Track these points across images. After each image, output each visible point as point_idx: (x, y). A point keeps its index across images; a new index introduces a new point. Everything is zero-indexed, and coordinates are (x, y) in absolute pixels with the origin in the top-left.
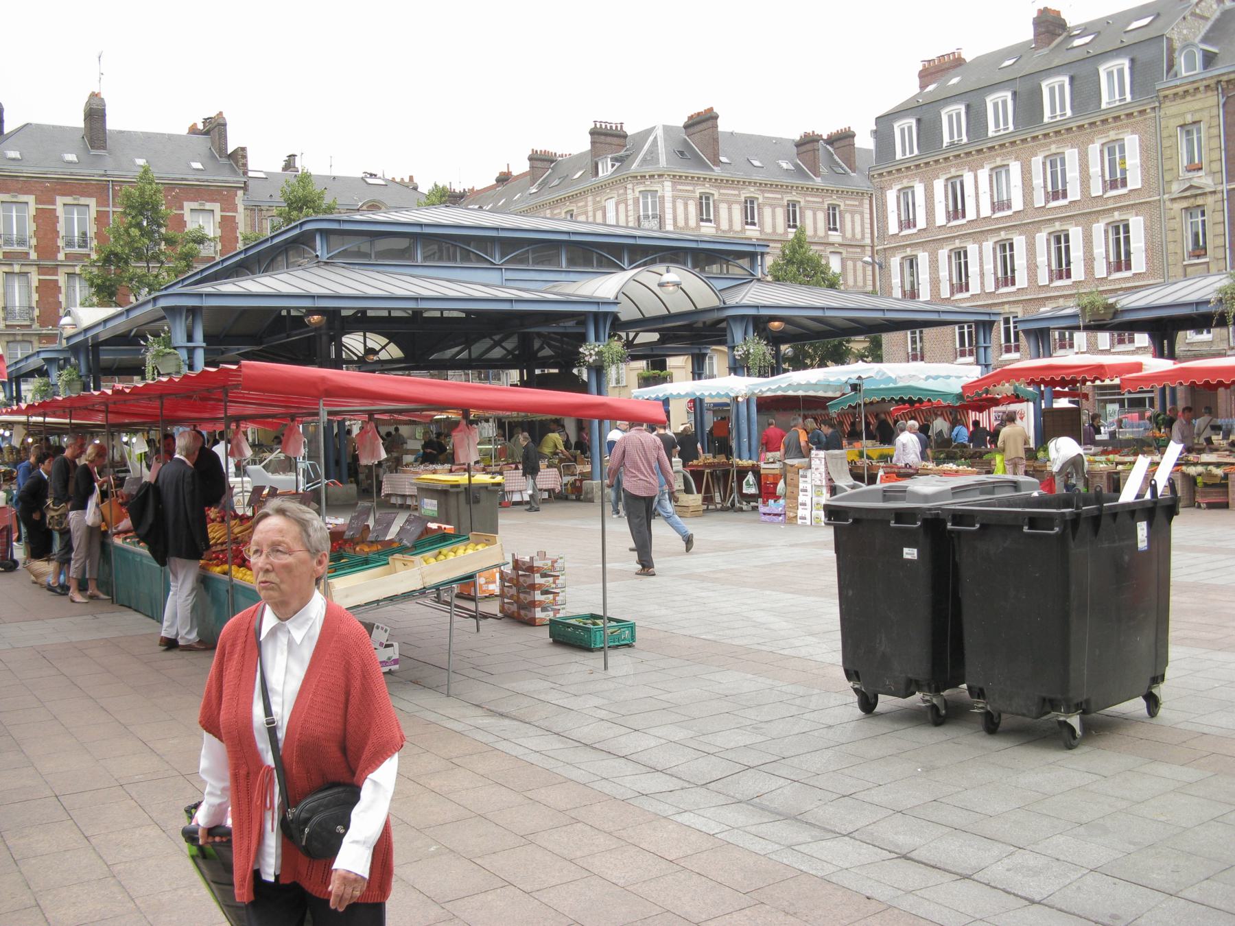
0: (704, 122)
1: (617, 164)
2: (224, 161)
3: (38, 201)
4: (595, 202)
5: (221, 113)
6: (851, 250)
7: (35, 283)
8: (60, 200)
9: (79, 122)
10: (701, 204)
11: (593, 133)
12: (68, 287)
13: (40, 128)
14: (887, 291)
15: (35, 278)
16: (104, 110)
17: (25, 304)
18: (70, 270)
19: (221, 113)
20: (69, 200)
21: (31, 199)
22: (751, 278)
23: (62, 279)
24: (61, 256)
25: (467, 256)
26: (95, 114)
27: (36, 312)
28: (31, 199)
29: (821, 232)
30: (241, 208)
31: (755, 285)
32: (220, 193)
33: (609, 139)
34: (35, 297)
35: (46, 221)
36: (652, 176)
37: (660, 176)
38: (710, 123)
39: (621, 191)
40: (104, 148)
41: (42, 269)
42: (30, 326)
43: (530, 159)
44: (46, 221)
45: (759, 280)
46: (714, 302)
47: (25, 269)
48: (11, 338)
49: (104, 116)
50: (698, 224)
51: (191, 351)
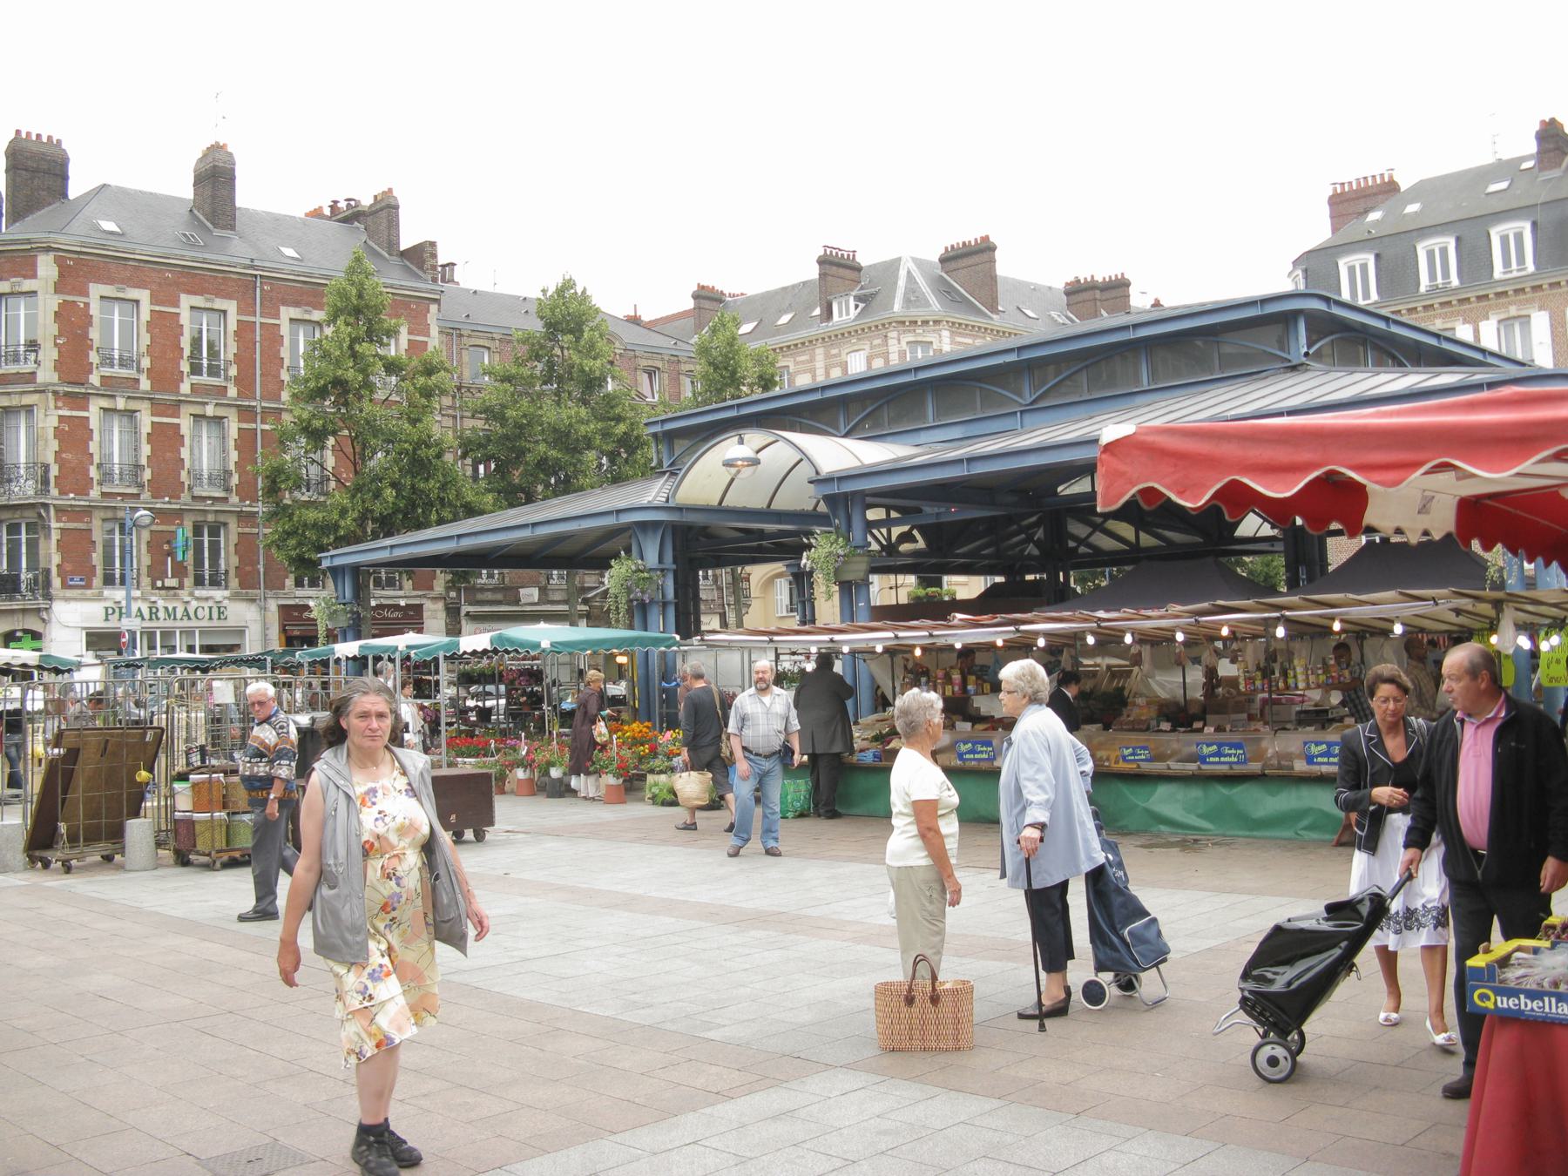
0: (983, 251)
1: (861, 305)
2: (395, 260)
3: (154, 300)
4: (827, 356)
5: (390, 190)
7: (146, 428)
8: (186, 301)
9: (184, 189)
11: (823, 262)
12: (192, 438)
13: (123, 192)
15: (146, 421)
16: (233, 170)
17: (128, 460)
18: (197, 410)
19: (390, 190)
20: (198, 301)
21: (143, 295)
23: (185, 424)
26: (216, 177)
27: (147, 475)
28: (143, 295)
30: (434, 331)
32: (407, 306)
33: (842, 271)
34: (146, 450)
35: (164, 326)
36: (925, 323)
37: (936, 322)
38: (985, 257)
39: (876, 342)
40: (233, 228)
41: (158, 408)
42: (225, 500)
43: (696, 297)
47: (133, 405)
48: (109, 514)
49: (233, 179)
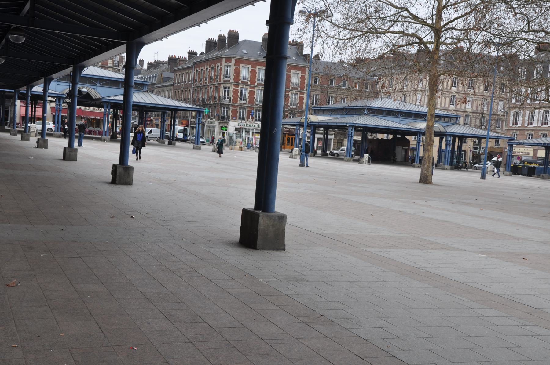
8: (258, 67)
14: (285, 117)
15: (249, 90)
20: (260, 67)
21: (250, 66)
22: (456, 123)
23: (255, 90)
24: (291, 88)
25: (393, 115)
28: (250, 66)
29: (447, 106)
30: (307, 73)
31: (456, 126)
41: (251, 87)
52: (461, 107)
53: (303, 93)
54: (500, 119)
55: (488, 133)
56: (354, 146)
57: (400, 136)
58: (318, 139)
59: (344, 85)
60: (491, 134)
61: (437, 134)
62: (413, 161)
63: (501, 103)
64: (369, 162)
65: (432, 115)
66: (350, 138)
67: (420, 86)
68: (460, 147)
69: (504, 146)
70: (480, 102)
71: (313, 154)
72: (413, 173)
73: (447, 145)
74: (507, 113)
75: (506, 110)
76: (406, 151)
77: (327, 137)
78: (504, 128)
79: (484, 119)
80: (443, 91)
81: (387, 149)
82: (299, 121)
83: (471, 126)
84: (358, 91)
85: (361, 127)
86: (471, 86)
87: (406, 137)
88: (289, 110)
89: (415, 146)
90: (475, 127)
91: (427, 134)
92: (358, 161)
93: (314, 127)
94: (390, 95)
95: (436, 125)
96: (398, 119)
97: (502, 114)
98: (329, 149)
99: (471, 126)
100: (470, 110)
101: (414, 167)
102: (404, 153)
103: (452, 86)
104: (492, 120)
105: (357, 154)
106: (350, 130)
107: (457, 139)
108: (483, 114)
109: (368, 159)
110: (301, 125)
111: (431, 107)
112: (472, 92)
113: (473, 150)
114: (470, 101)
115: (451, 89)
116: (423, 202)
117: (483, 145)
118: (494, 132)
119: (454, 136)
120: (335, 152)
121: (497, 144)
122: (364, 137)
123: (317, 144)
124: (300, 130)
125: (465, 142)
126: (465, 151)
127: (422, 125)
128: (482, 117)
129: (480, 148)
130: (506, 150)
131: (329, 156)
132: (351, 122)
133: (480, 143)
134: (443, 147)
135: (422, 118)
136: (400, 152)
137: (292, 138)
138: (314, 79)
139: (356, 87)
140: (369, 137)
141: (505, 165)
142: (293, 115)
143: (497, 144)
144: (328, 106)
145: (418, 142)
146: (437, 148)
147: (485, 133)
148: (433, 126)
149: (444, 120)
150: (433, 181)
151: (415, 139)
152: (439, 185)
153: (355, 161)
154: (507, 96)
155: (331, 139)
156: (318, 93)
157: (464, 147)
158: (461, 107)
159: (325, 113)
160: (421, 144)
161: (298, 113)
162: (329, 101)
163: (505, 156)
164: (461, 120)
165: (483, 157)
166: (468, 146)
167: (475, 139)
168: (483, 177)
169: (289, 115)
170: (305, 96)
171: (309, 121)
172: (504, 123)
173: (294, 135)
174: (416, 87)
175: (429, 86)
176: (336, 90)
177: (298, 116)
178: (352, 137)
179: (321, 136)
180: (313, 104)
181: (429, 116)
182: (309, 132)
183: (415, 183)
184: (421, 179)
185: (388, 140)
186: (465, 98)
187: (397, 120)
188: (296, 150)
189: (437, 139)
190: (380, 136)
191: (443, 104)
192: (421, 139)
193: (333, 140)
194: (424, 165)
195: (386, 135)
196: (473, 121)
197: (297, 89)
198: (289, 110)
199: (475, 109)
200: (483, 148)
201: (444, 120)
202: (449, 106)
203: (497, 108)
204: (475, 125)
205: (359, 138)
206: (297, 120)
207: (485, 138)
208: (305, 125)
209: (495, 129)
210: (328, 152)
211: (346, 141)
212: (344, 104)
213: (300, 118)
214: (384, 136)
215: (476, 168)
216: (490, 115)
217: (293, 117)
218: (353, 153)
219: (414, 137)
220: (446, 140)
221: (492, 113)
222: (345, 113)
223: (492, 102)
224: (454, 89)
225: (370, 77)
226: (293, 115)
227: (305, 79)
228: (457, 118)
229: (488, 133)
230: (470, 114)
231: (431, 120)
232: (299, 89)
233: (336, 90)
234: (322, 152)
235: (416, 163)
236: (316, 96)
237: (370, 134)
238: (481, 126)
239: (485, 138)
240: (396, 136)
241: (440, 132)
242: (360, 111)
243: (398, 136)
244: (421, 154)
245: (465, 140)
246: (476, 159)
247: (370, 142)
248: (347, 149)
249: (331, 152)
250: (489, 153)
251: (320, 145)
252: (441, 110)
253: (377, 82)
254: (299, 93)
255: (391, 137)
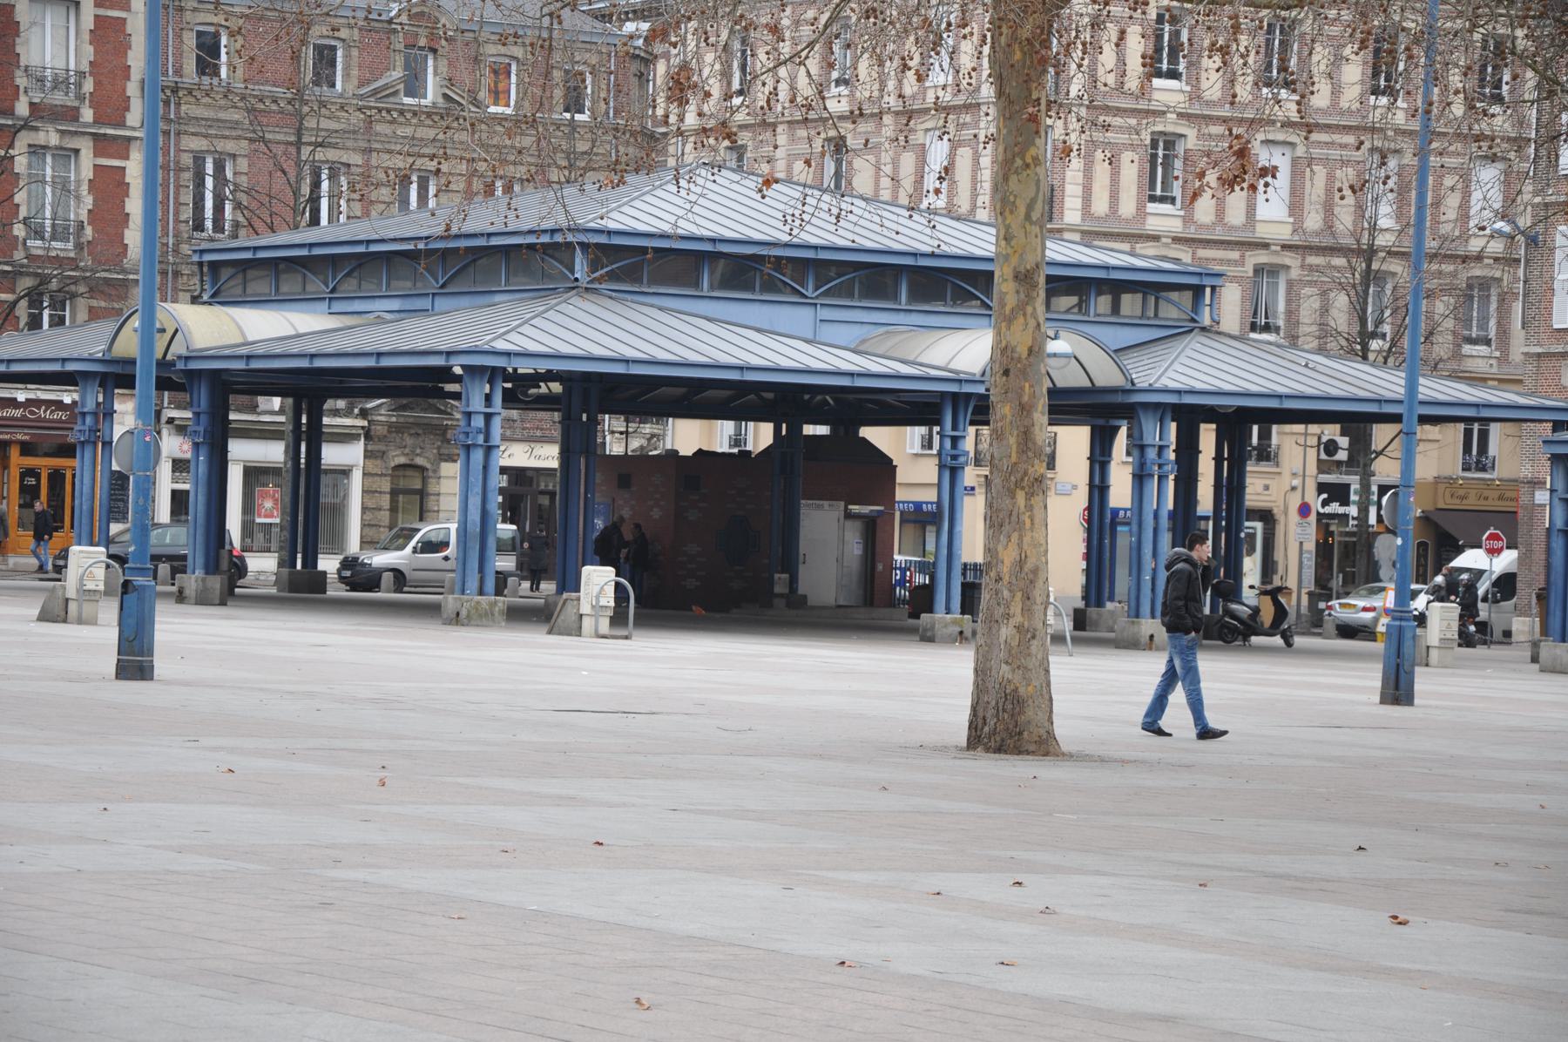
6: (1313, 260)
10: (1154, 157)
24: (22, 108)
25: (770, 286)
29: (1128, 207)
31: (1196, 343)
35: (1022, 191)
44: (1022, 191)
45: (1203, 329)
46: (1116, 380)
50: (1141, 209)
51: (488, 417)
52: (1220, 211)
53: (121, 147)
54: (1485, 284)
55: (1412, 386)
56: (512, 511)
57: (827, 434)
58: (253, 474)
59: (414, 84)
60: (1433, 388)
61: (1069, 405)
62: (923, 600)
63: (1488, 175)
64: (619, 618)
65: (1024, 278)
66: (478, 456)
67: (937, 77)
68: (1231, 488)
69: (1526, 472)
70: (1346, 176)
71: (216, 583)
72: (929, 681)
73: (1140, 478)
74: (1532, 241)
75: (1525, 221)
76: (874, 534)
77: (315, 455)
78: (1519, 345)
79: (1377, 292)
80: (1098, 110)
81: (729, 524)
82: (98, 350)
83: (1293, 340)
84: (519, 123)
85: (550, 376)
86: (1281, 74)
87: (867, 433)
88: (18, 273)
89: (930, 496)
90: (1321, 350)
91: (1003, 411)
92: (541, 616)
93: (216, 394)
94: (739, 151)
95: (1053, 346)
96: (806, 313)
97: (1497, 247)
98: (337, 543)
99: (1293, 340)
100: (1284, 233)
101: (928, 638)
102: (854, 547)
103: (1153, 68)
104: (1430, 295)
105: (533, 571)
106: (477, 404)
107: (1207, 437)
108: (1370, 253)
109: (609, 600)
110: (117, 376)
111: (1015, 222)
112: (1291, 111)
113: (1316, 503)
114: (1271, 171)
115: (1144, 92)
116: (993, 889)
117: (1386, 470)
118: (1456, 376)
119: (1189, 415)
120: (380, 559)
121: (1476, 455)
122: (578, 443)
123: (248, 507)
124: (109, 414)
125: (1265, 454)
126: (1266, 516)
127: (961, 350)
128: (1369, 277)
129: (1365, 487)
130: (1542, 497)
131: (336, 590)
132: (482, 342)
133: (1362, 455)
134: (1120, 493)
135: (963, 296)
136: (826, 538)
137: (57, 478)
138: (190, 40)
139: (498, 95)
140: (615, 447)
141: (1542, 597)
142: (57, 305)
143: (1476, 455)
144: (312, 235)
145: (951, 469)
146: (1081, 499)
147: (1385, 383)
148: (1036, 351)
149: (1116, 309)
150: (1061, 729)
151: (928, 444)
152: (1102, 760)
153: (519, 615)
154: (1521, 122)
155: (345, 472)
156: (230, 146)
157: (1259, 488)
158: (1220, 211)
159: (289, 285)
160: (970, 475)
161: (93, 291)
162: (314, 200)
163: (1539, 534)
164: (1230, 305)
165: (1387, 548)
166: (1287, 481)
167: (1331, 431)
168: (1398, 690)
169: (22, 310)
170: (134, 168)
171: (178, 349)
172: (1518, 308)
173: (68, 451)
174: (910, 85)
175: (999, 79)
176: (356, 118)
177: (94, 315)
178: (489, 449)
179: (273, 453)
180: (199, 226)
181: (1005, 286)
182: (181, 430)
183: (942, 750)
184: (975, 726)
185: (741, 460)
186: (1242, 153)
187: (799, 317)
188: (87, 563)
189: (1074, 441)
190: (687, 436)
191: (1098, 203)
192: (968, 445)
193: (357, 478)
194: (993, 622)
195: (727, 427)
196: (1309, 305)
197: (72, 114)
198: (18, 273)
199: (1313, 221)
200: (1383, 489)
201: (1116, 309)
202: (1141, 213)
203: (1464, 206)
204: (1325, 332)
205: (547, 456)
206: (82, 341)
207: (1396, 418)
208: (145, 377)
209: (1457, 355)
210: (328, 564)
211: (449, 480)
212: (418, 220)
213: (109, 327)
214: (717, 436)
215: (1348, 631)
216: (1415, 257)
217: (58, 322)
218: (507, 563)
219: (921, 430)
220: (1137, 446)
221: (1431, 245)
222: (433, 285)
223: (1423, 170)
224: (1167, 92)
225: (590, 24)
226: (57, 305)
227: (124, 47)
228: (1198, 291)
229: (1412, 386)
230: (1288, 259)
231: (1021, 308)
232: (87, 115)
233: (356, 118)
234: (287, 562)
235: (939, 615)
236: (219, 168)
237: (618, 423)
238: (1365, 336)
239: (1396, 418)
240: (795, 430)
241: (1094, 390)
242: (535, 263)
243: (809, 430)
244: (972, 544)
245: (1265, 435)
246: (1345, 559)
247: (624, 481)
248: (463, 532)
249: (349, 563)
250: (1426, 520)
251: (271, 512)
252: (1089, 237)
253: (648, 60)
254: (86, 147)
255: (761, 436)
